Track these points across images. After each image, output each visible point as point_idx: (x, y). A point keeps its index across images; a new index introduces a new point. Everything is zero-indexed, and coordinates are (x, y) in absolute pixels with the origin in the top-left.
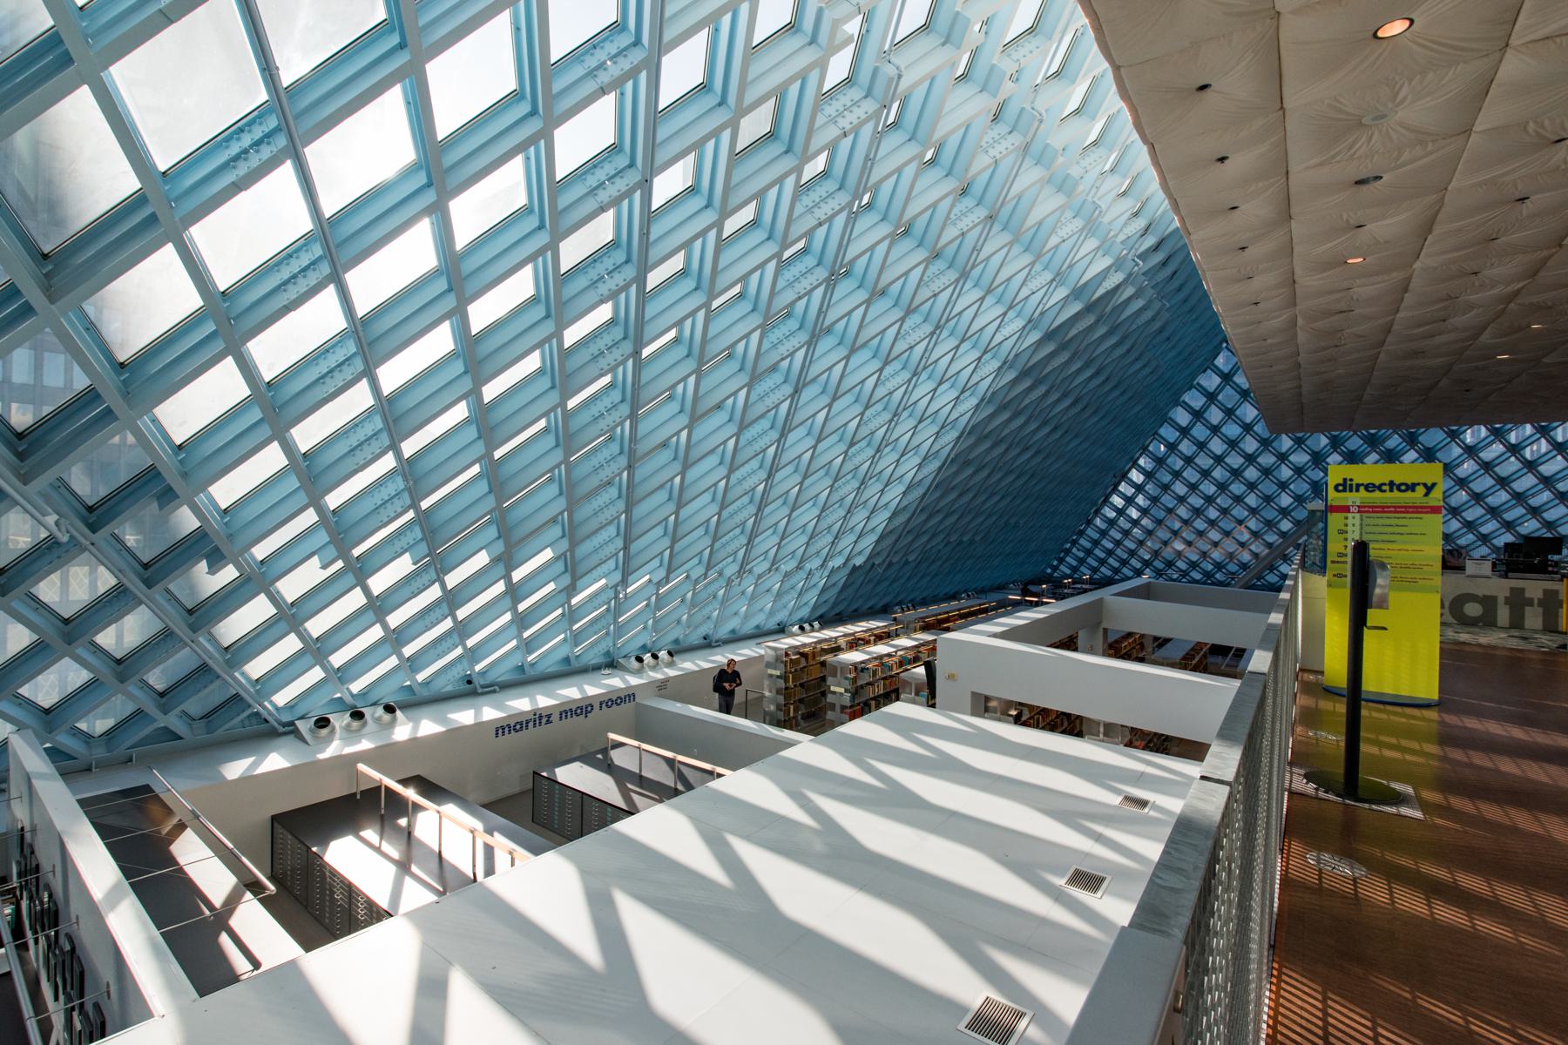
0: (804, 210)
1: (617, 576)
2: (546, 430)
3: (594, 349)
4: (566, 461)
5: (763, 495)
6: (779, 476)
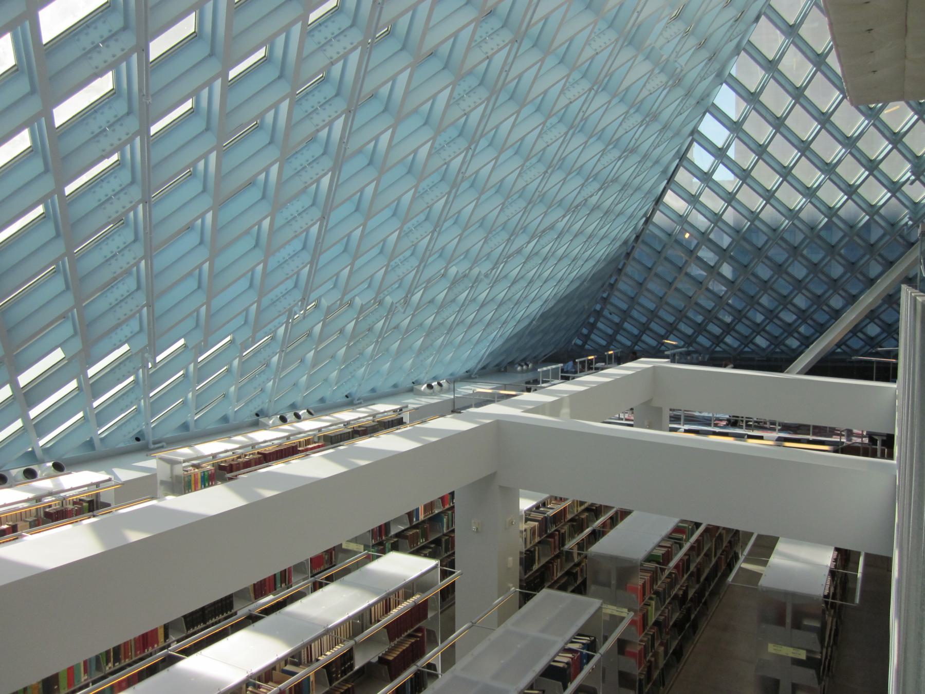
0: (316, 47)
1: (142, 340)
2: (43, 217)
3: (85, 42)
4: (69, 253)
5: (317, 239)
6: (324, 259)
